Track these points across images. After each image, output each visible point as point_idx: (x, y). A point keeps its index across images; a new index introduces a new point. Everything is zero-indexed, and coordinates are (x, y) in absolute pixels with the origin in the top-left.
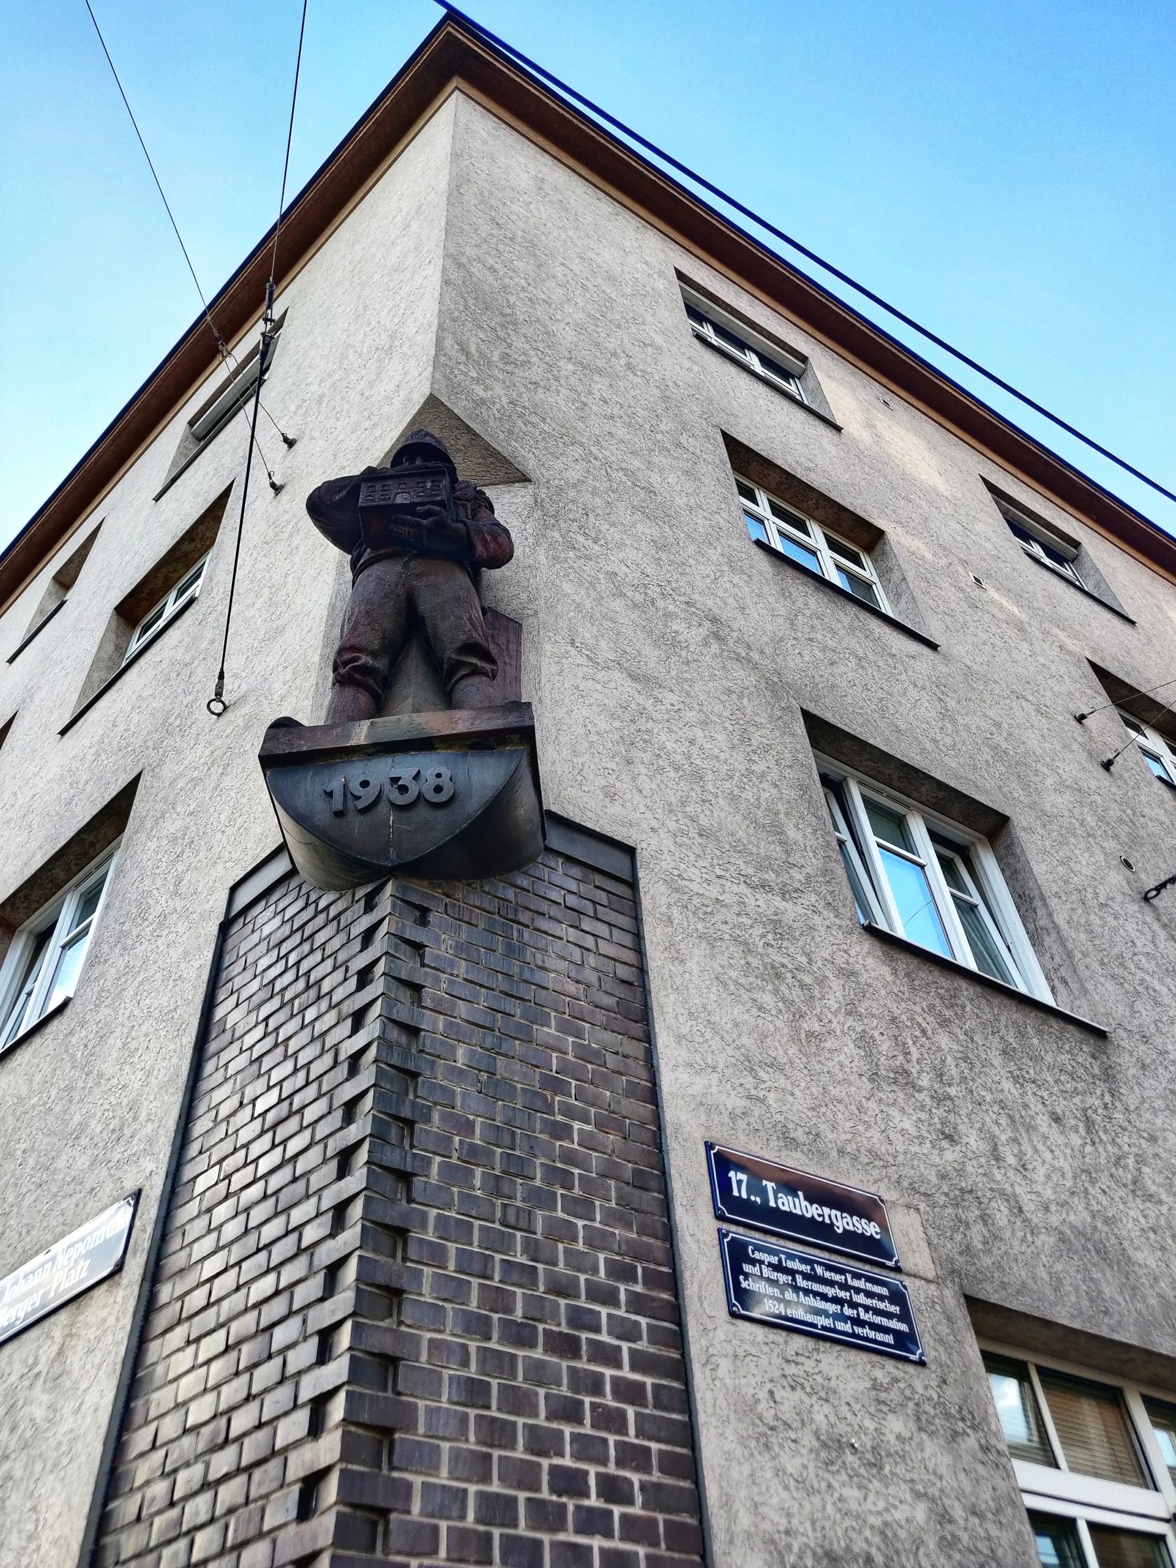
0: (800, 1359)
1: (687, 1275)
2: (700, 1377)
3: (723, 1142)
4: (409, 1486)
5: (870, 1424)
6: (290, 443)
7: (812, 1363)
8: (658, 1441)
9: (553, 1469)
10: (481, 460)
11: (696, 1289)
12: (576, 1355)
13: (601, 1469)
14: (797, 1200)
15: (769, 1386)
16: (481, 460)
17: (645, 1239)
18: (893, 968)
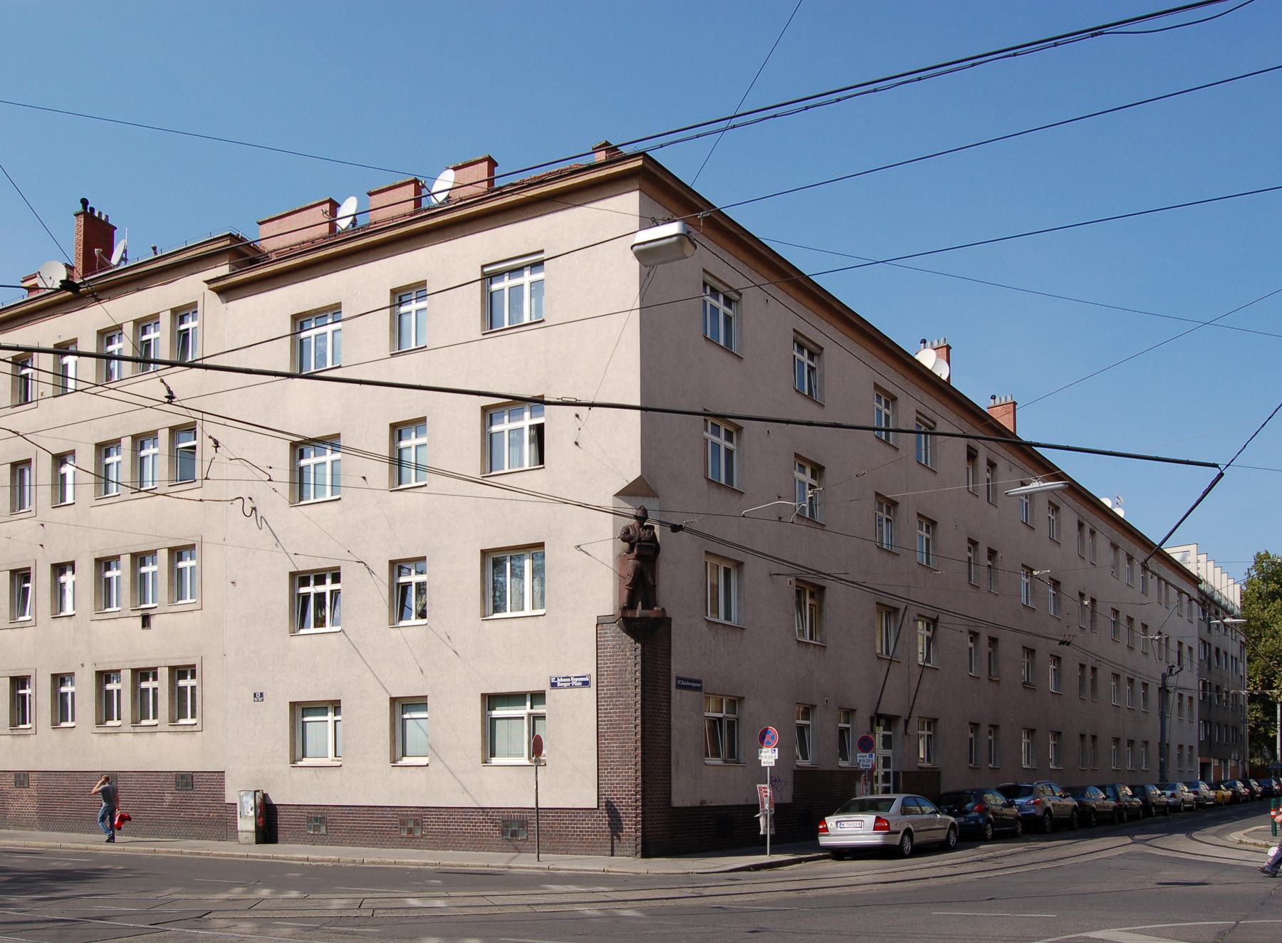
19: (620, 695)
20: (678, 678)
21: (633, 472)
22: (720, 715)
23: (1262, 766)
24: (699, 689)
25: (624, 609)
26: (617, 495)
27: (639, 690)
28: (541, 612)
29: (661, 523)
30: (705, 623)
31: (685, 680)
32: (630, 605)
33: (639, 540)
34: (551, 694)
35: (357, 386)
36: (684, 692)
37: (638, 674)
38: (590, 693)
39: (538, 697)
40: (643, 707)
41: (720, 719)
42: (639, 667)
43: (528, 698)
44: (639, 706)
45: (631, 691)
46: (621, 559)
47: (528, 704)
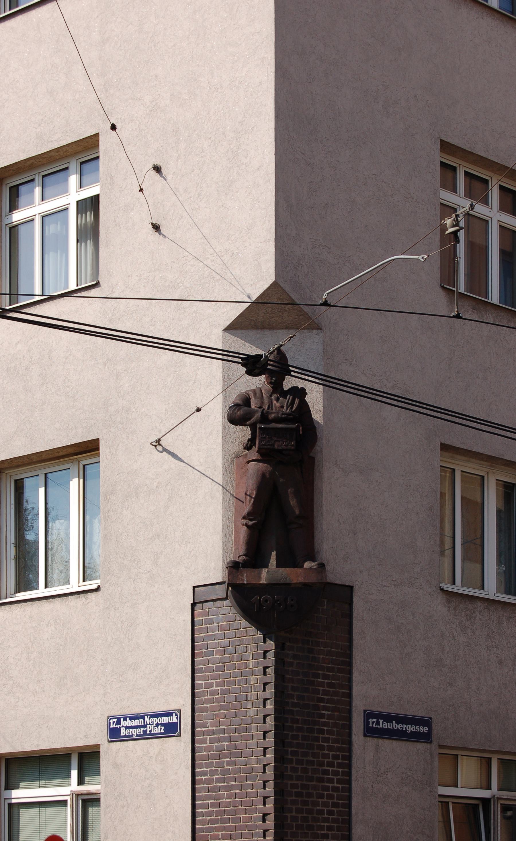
0: (382, 775)
1: (354, 756)
2: (354, 784)
3: (369, 709)
4: (287, 816)
5: (398, 790)
6: (157, 169)
7: (385, 775)
8: (341, 800)
9: (317, 810)
10: (296, 317)
11: (356, 760)
12: (323, 782)
13: (327, 808)
14: (391, 724)
15: (372, 784)
16: (296, 317)
17: (343, 746)
18: (449, 607)
19: (234, 752)
20: (368, 715)
21: (255, 272)
22: (485, 794)
23: (31, 580)
24: (426, 738)
25: (234, 567)
26: (223, 330)
27: (271, 739)
28: (92, 585)
29: (328, 381)
30: (440, 598)
31: (389, 718)
32: (252, 555)
33: (264, 418)
34: (111, 753)
35: (122, 297)
36: (387, 744)
37: (270, 706)
38: (179, 747)
39: (88, 760)
40: (279, 775)
41: (486, 802)
42: (271, 691)
43: (75, 762)
44: (270, 772)
45: (256, 743)
46: (235, 463)
47: (74, 774)
